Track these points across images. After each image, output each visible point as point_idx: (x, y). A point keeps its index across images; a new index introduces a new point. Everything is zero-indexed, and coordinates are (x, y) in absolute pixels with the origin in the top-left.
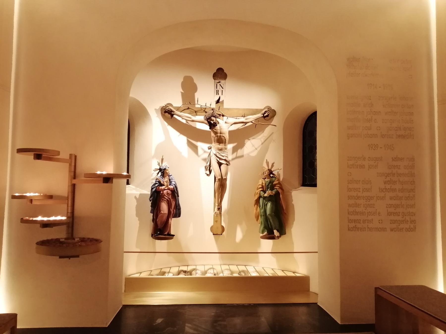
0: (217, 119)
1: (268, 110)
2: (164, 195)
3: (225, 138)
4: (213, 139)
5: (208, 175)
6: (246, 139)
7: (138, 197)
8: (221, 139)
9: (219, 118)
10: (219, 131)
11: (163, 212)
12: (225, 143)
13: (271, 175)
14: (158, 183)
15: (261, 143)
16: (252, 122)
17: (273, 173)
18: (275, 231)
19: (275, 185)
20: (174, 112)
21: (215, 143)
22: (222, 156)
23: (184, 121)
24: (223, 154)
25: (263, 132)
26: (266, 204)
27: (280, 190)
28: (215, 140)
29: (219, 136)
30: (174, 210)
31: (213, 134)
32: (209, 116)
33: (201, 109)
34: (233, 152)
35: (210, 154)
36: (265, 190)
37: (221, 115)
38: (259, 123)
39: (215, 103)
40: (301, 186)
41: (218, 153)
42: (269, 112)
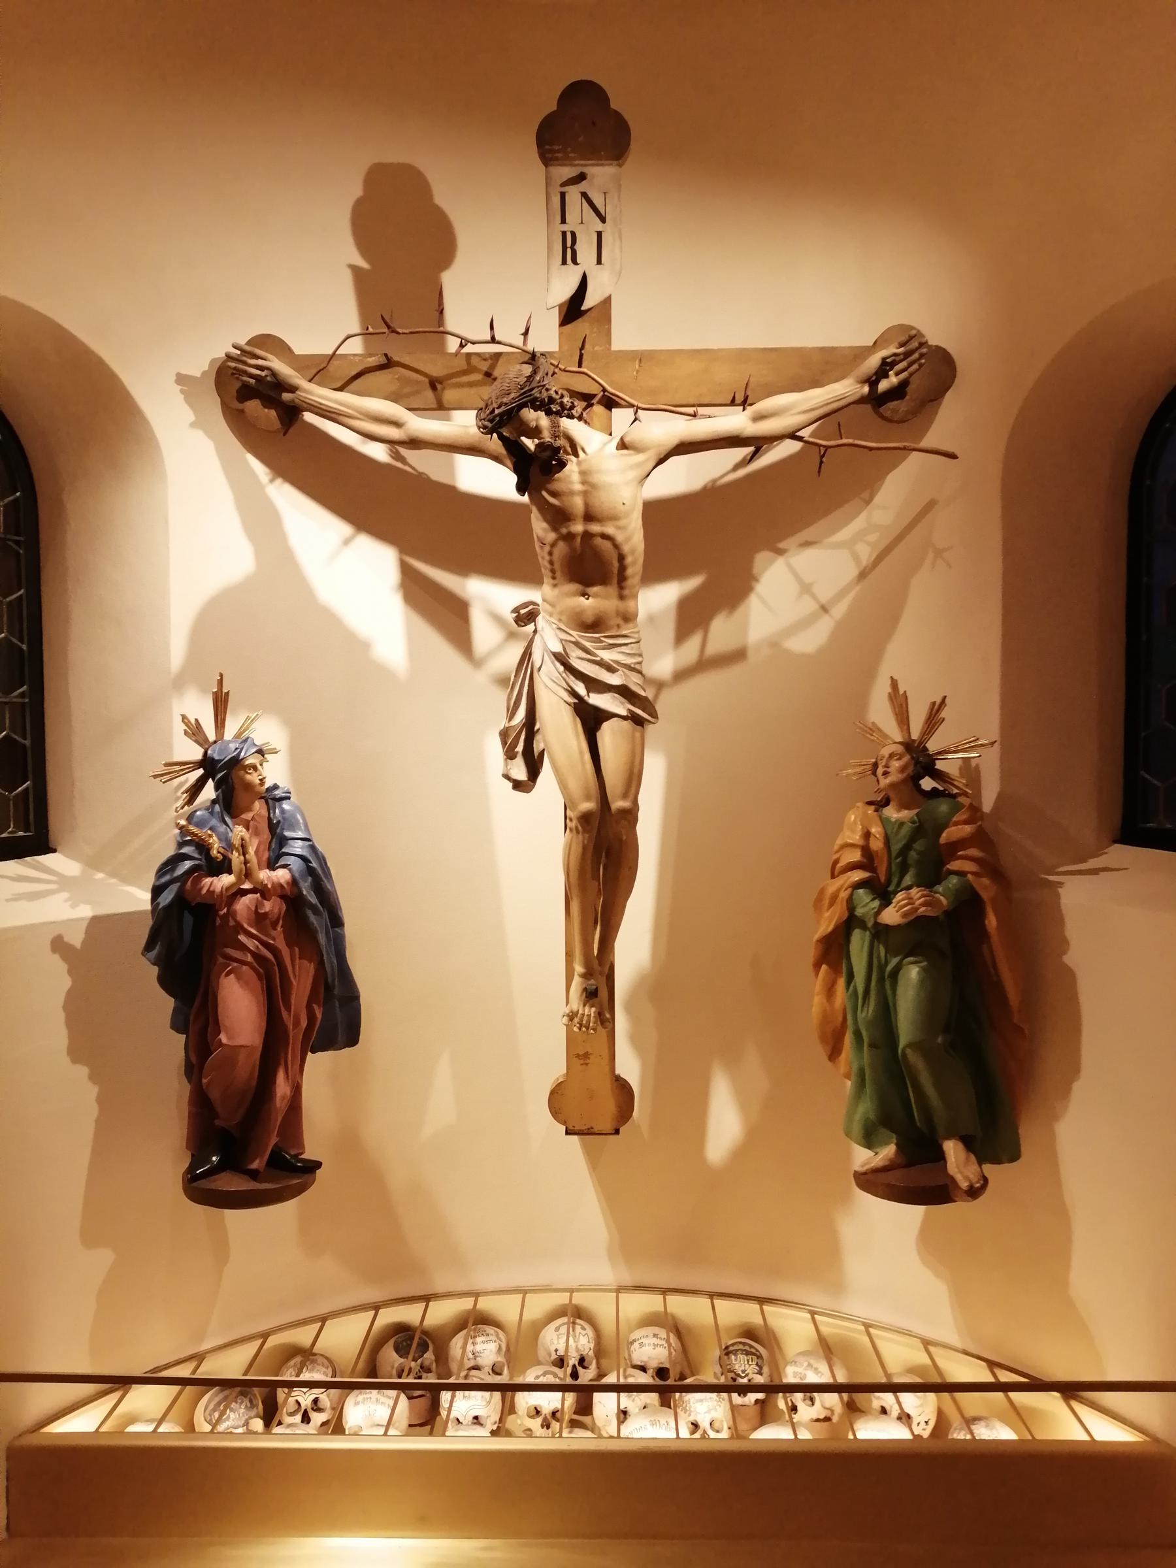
0: (565, 423)
1: (902, 350)
2: (239, 928)
3: (616, 546)
4: (544, 562)
5: (518, 785)
6: (758, 550)
7: (76, 938)
8: (597, 555)
9: (580, 418)
10: (578, 504)
11: (229, 1038)
12: (622, 578)
13: (927, 784)
14: (196, 856)
15: (853, 572)
16: (800, 439)
17: (939, 765)
18: (952, 1149)
19: (954, 848)
20: (293, 389)
21: (555, 586)
22: (602, 664)
23: (378, 452)
24: (607, 656)
25: (868, 502)
26: (889, 968)
27: (986, 881)
28: (557, 566)
29: (579, 540)
30: (315, 1006)
31: (539, 526)
32: (505, 400)
33: (468, 363)
34: (682, 634)
35: (527, 655)
36: (883, 878)
37: (594, 396)
38: (844, 441)
39: (555, 317)
40: (1115, 842)
41: (577, 644)
42: (910, 365)
